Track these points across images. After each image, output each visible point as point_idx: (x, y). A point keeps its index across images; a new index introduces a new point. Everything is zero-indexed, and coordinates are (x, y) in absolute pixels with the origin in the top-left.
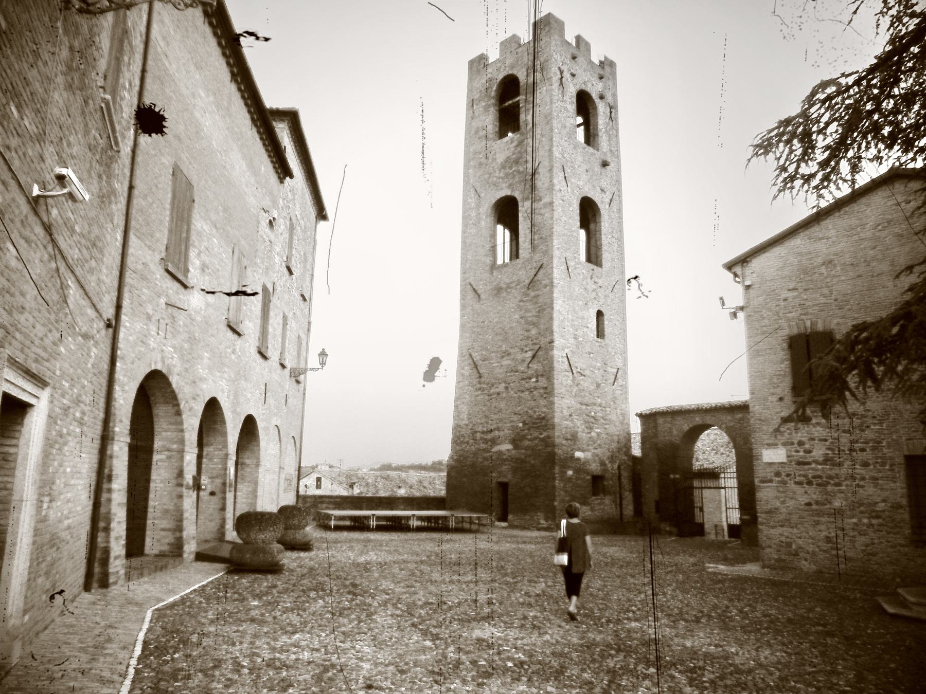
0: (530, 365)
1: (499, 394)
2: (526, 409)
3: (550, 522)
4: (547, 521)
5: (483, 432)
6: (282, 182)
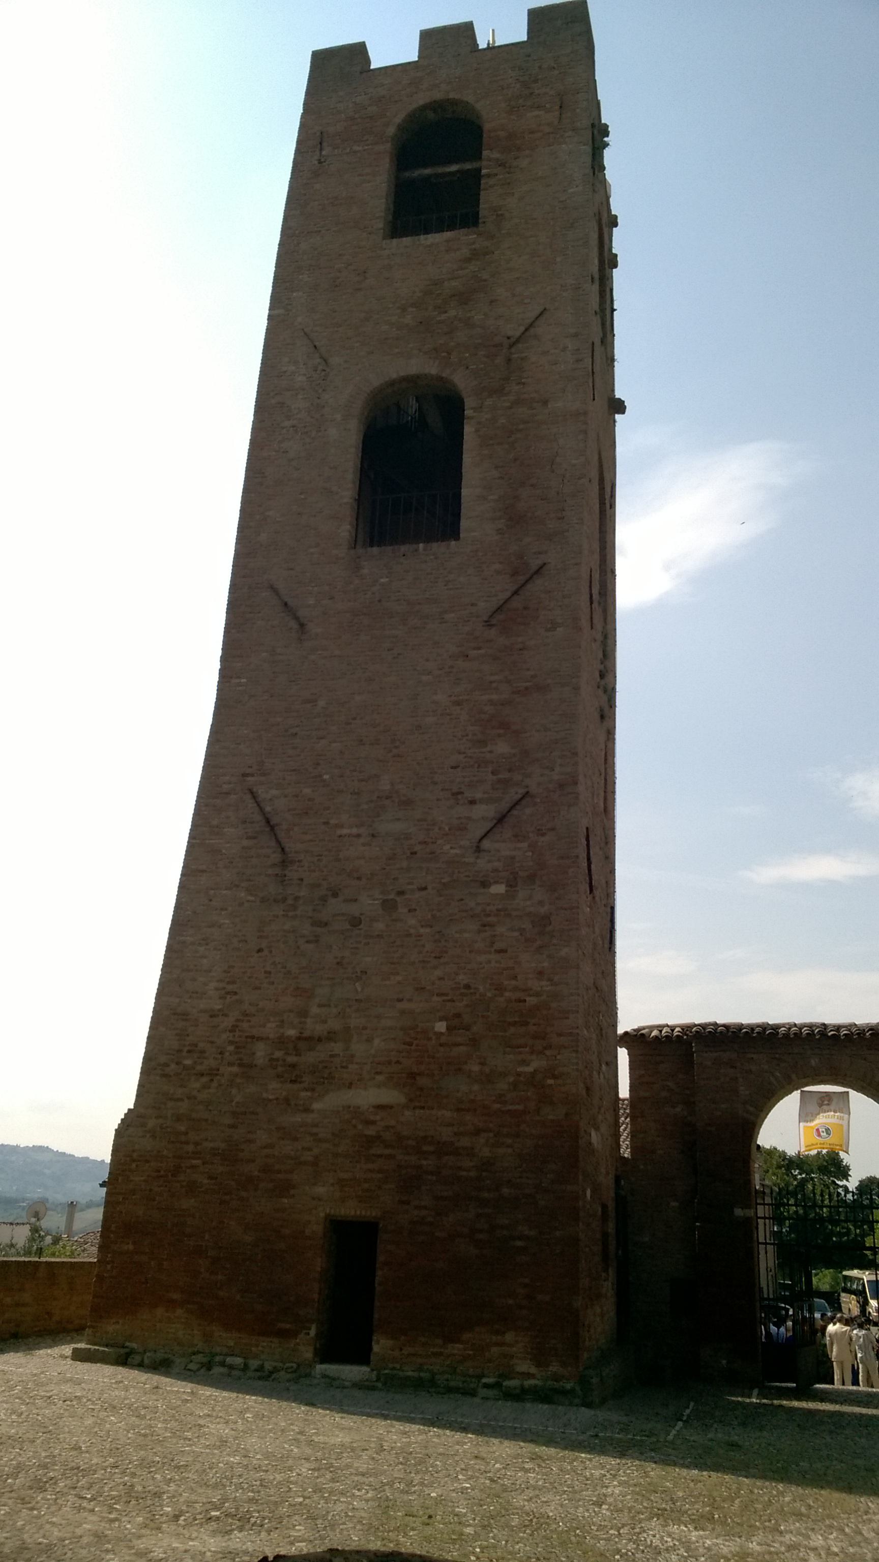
0: (486, 844)
1: (355, 922)
2: (462, 979)
3: (554, 1368)
4: (539, 1363)
5: (281, 1042)
6: (101, 1185)
